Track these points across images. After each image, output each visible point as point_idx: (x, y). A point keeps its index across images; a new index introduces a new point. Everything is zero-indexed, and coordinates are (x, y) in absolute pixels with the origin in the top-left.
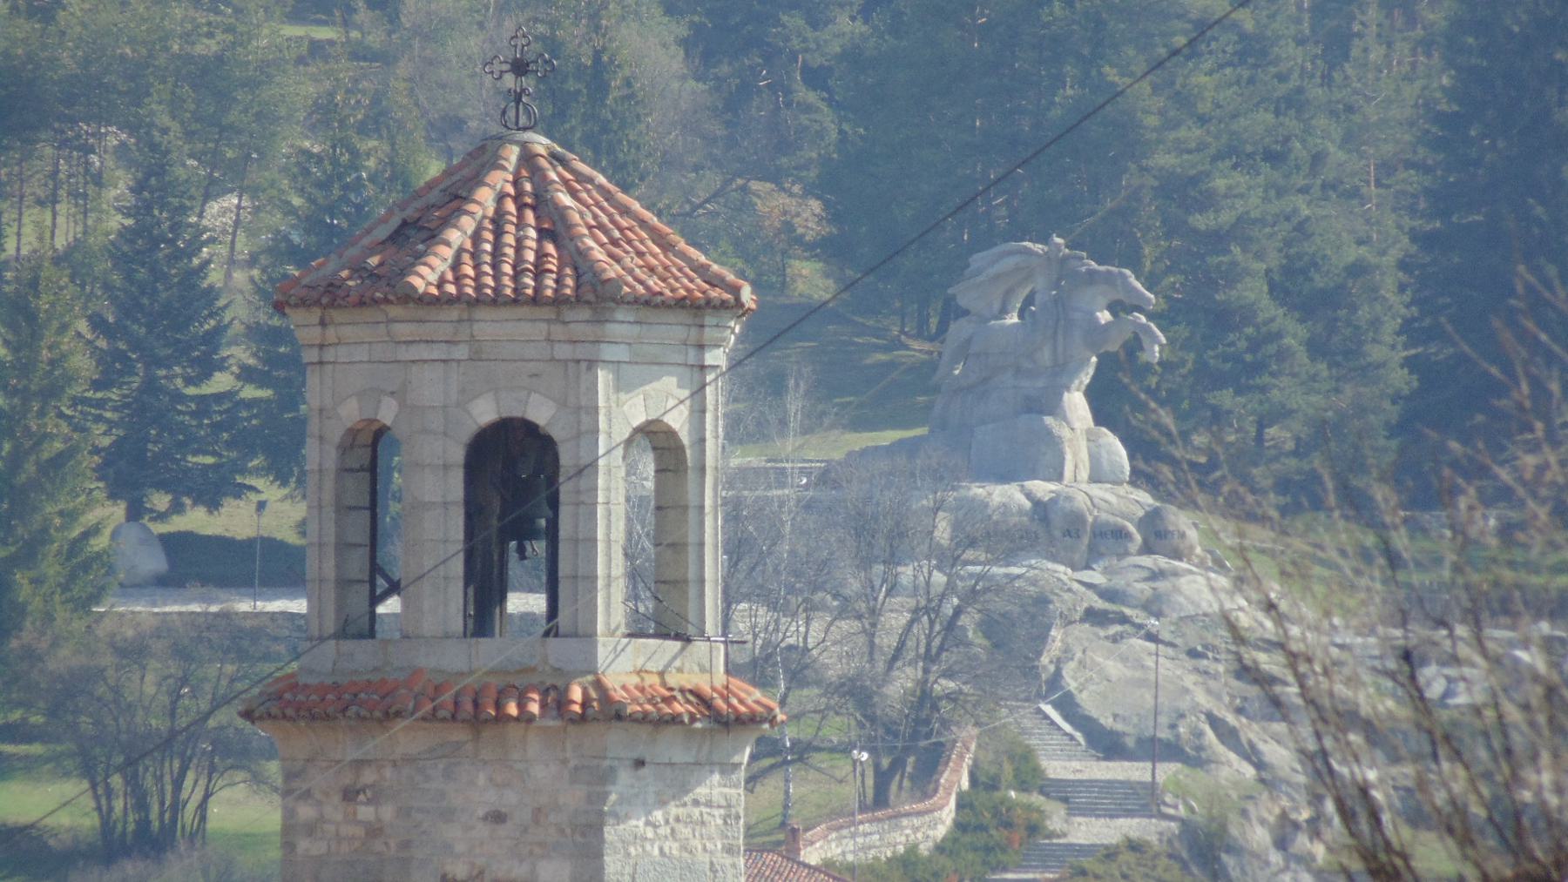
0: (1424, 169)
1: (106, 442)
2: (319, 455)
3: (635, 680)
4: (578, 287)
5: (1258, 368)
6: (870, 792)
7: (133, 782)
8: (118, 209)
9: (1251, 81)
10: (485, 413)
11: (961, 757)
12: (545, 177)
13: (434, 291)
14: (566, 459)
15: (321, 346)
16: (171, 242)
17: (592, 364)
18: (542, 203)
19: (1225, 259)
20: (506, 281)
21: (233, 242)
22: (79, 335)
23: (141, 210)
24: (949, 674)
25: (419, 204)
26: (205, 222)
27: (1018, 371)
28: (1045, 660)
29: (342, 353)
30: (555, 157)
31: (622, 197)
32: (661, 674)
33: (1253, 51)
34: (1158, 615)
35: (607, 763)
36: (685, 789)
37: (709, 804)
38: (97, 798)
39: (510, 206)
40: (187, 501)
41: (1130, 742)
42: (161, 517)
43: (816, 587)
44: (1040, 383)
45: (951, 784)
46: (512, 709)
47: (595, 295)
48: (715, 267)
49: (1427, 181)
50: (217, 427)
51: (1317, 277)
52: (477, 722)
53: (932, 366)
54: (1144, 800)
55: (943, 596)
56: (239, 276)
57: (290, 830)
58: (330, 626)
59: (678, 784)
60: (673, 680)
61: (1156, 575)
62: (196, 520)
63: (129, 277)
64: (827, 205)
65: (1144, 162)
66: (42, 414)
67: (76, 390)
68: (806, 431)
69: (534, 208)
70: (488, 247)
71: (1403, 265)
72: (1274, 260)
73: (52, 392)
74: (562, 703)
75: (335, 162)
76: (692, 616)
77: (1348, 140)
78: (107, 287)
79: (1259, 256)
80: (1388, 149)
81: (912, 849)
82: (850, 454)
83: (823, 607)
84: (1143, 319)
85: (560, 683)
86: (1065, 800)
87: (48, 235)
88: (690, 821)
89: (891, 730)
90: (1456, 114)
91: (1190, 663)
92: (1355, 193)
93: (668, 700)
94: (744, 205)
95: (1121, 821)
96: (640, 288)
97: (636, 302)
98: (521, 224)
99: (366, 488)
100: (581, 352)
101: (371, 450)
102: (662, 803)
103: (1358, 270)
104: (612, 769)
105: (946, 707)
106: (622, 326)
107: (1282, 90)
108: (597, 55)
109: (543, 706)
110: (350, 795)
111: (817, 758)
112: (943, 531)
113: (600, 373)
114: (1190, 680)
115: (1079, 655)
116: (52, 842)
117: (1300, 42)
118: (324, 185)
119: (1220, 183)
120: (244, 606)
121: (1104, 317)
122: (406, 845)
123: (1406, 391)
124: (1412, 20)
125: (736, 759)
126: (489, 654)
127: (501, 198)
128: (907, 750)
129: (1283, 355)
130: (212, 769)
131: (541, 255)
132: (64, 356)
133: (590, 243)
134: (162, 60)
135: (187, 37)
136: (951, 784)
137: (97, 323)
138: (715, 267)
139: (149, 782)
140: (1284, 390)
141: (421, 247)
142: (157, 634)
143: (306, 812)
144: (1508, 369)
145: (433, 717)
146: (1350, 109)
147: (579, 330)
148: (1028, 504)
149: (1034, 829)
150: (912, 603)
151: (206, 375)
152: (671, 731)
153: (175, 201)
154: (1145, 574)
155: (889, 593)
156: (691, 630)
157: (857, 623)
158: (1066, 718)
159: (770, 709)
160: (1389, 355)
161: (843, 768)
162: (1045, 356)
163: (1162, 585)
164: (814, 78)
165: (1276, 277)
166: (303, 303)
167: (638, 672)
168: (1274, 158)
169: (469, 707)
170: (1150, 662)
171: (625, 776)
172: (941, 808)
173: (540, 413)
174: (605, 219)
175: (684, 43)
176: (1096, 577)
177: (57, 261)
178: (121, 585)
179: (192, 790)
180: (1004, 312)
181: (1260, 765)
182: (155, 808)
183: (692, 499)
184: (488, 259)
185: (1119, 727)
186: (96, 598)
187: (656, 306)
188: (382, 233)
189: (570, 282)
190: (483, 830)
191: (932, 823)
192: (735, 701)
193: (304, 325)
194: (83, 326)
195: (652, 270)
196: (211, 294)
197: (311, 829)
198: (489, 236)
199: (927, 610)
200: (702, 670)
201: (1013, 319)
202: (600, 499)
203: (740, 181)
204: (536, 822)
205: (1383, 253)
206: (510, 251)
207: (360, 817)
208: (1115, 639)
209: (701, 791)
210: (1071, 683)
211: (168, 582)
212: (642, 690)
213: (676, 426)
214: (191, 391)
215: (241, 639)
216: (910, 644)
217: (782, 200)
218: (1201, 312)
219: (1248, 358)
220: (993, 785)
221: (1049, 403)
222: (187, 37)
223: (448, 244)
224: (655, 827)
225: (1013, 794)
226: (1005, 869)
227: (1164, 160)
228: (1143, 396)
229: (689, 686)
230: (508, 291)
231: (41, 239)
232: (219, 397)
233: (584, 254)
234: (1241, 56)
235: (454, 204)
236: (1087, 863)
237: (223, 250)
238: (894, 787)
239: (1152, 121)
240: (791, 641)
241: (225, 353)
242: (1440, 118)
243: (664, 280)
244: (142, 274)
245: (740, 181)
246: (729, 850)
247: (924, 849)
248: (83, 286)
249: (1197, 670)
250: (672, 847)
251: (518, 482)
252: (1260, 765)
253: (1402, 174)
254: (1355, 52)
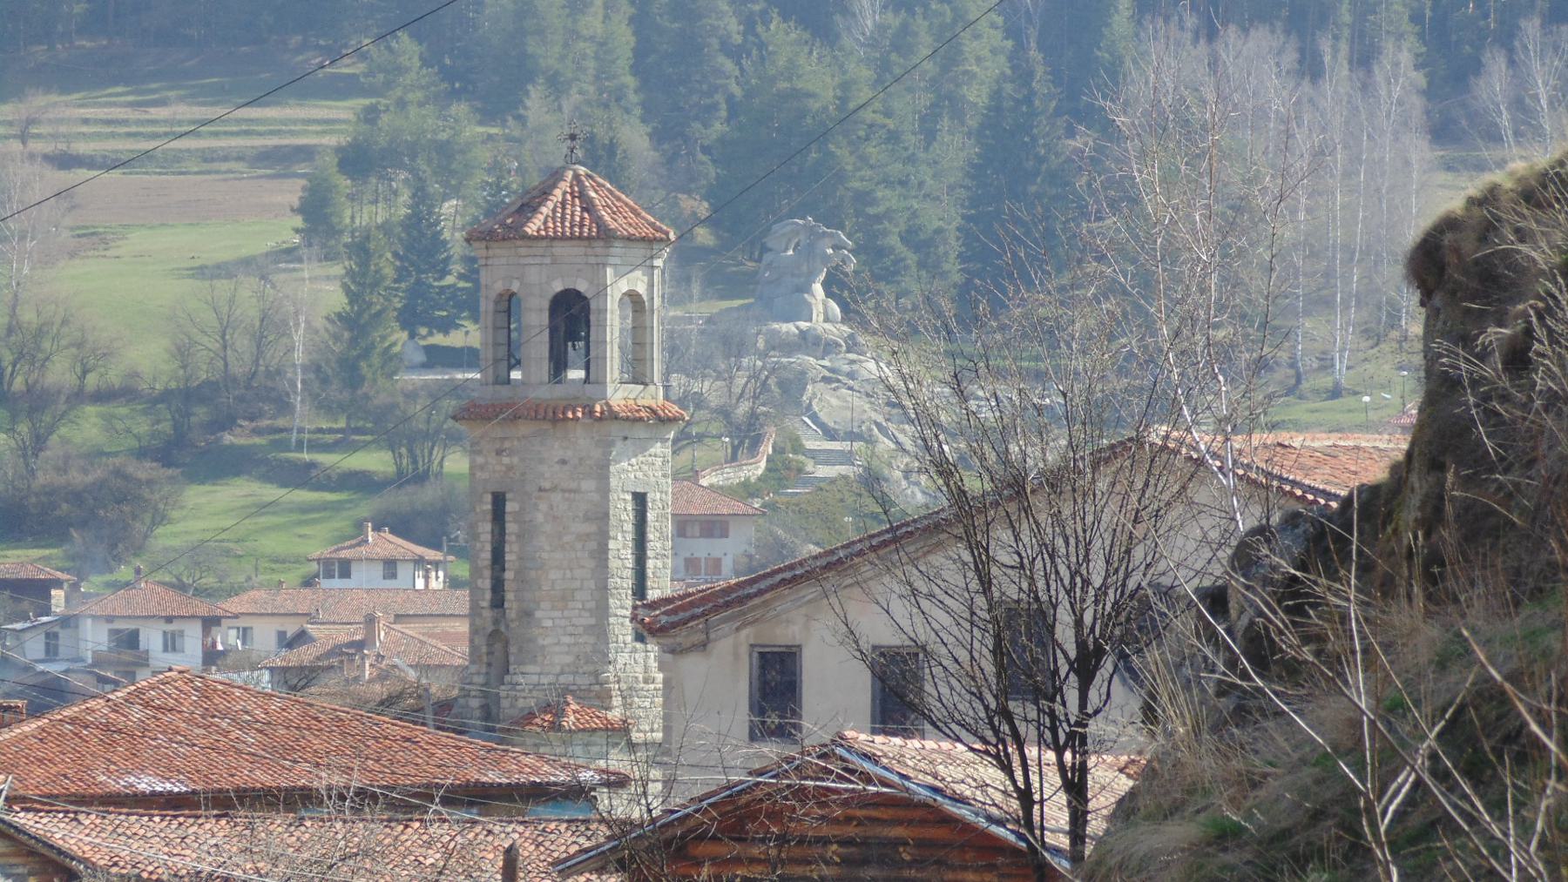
2: (486, 306)
5: (897, 273)
7: (410, 451)
10: (558, 287)
14: (593, 306)
17: (605, 265)
18: (582, 195)
27: (793, 275)
30: (588, 176)
33: (893, 137)
39: (569, 197)
42: (424, 338)
46: (570, 415)
47: (605, 235)
52: (555, 421)
53: (756, 273)
54: (847, 458)
56: (457, 235)
58: (491, 380)
61: (853, 362)
62: (438, 339)
67: (388, 283)
68: (701, 300)
71: (958, 229)
72: (903, 227)
73: (375, 285)
74: (592, 412)
78: (400, 239)
80: (952, 180)
89: (738, 428)
94: (676, 204)
97: (623, 238)
101: (508, 305)
103: (939, 231)
105: (762, 418)
106: (617, 249)
107: (905, 154)
110: (499, 453)
112: (761, 344)
117: (914, 133)
119: (879, 194)
120: (459, 376)
121: (830, 251)
122: (523, 474)
124: (963, 123)
126: (559, 391)
127: (565, 193)
129: (907, 268)
130: (445, 446)
131: (582, 219)
137: (396, 255)
139: (418, 452)
140: (908, 282)
143: (480, 460)
144: (1001, 246)
147: (599, 251)
149: (800, 470)
151: (441, 278)
152: (639, 425)
161: (718, 444)
162: (805, 268)
163: (855, 367)
164: (706, 150)
166: (479, 239)
168: (903, 183)
171: (619, 444)
173: (582, 287)
175: (650, 135)
176: (826, 363)
177: (378, 227)
180: (786, 249)
181: (897, 443)
182: (898, 832)
183: (648, 324)
186: (395, 373)
188: (513, 208)
190: (557, 467)
194: (389, 255)
196: (445, 242)
197: (482, 468)
201: (791, 252)
209: (652, 451)
210: (816, 408)
211: (427, 366)
215: (456, 389)
218: (870, 250)
220: (782, 451)
221: (806, 288)
222: (434, 132)
227: (856, 185)
232: (449, 287)
233: (600, 218)
234: (888, 141)
244: (415, 233)
246: (664, 476)
247: (753, 480)
250: (639, 475)
251: (572, 317)
252: (897, 443)
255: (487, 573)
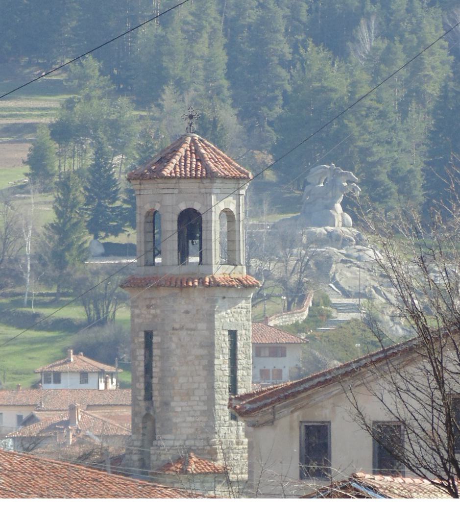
0: (427, 145)
1: (88, 219)
2: (140, 218)
3: (223, 276)
4: (207, 174)
5: (386, 197)
6: (286, 307)
7: (96, 307)
8: (91, 159)
9: (382, 123)
10: (183, 207)
11: (309, 298)
12: (198, 146)
13: (169, 175)
14: (204, 217)
15: (140, 190)
16: (105, 167)
17: (210, 194)
18: (197, 152)
19: (376, 169)
20: (188, 172)
21: (121, 168)
22: (81, 192)
23: (96, 160)
24: (306, 277)
25: (165, 153)
26: (113, 162)
28: (331, 272)
29: (146, 192)
30: (201, 140)
31: (218, 150)
32: (229, 274)
33: (382, 115)
34: (360, 260)
35: (215, 298)
36: (236, 304)
37: (242, 308)
38: (86, 311)
39: (189, 153)
40: (109, 234)
41: (353, 294)
42: (103, 238)
43: (272, 254)
44: (329, 201)
45: (307, 305)
46: (191, 284)
47: (211, 176)
48: (242, 168)
49: (428, 148)
50: (117, 215)
51: (400, 173)
52: (181, 287)
53: (301, 197)
54: (357, 308)
55: (304, 256)
56: (122, 176)
57: (133, 316)
59: (234, 303)
60: (232, 276)
61: (360, 250)
62: (112, 239)
63: (94, 176)
64: (273, 156)
65: (355, 144)
66: (71, 212)
67: (80, 206)
68: (268, 214)
69: (195, 153)
70: (183, 164)
71: (422, 170)
72: (389, 169)
73: (74, 206)
74: (204, 282)
75: (146, 146)
76: (237, 259)
77: (408, 138)
78: (88, 179)
79: (385, 168)
80: (418, 141)
81: (297, 322)
82: (280, 220)
83: (274, 259)
84: (355, 185)
85: (203, 277)
86: (336, 309)
87: (72, 166)
88: (237, 313)
89: (291, 291)
90: (436, 131)
91: (368, 273)
92: (409, 152)
93: (231, 281)
94: (252, 157)
95: (351, 314)
96: (223, 174)
98: (191, 158)
99: (152, 227)
100: (208, 191)
101: (153, 217)
102: (230, 308)
103: (410, 171)
104: (216, 299)
105: (305, 285)
106: (218, 184)
107: (390, 125)
108: (214, 119)
109: (198, 283)
110: (148, 307)
111: (273, 299)
112: (304, 240)
113: (213, 196)
114: (368, 277)
115: (340, 271)
116: (75, 323)
117: (395, 113)
118: (144, 152)
119: (374, 150)
120: (125, 261)
121: (345, 184)
122: (163, 320)
123: (423, 202)
124: (424, 107)
125: (249, 296)
126: (184, 269)
127: (186, 151)
128: (295, 296)
129: (391, 194)
131: (197, 166)
132: (77, 197)
133: (210, 162)
134: (102, 120)
135: (108, 115)
136: (307, 305)
137: (86, 189)
138: (242, 168)
139: (100, 307)
140: (392, 202)
141: (165, 164)
142: (102, 268)
143: (137, 311)
145: (170, 286)
146: (408, 130)
147: (207, 185)
148: (326, 233)
149: (328, 316)
150: (297, 258)
151: (114, 202)
153: (105, 157)
154: (433, 438)
155: (290, 256)
156: (237, 263)
157: (282, 264)
158: (337, 288)
159: (258, 283)
160: (419, 194)
161: (279, 301)
163: (361, 253)
164: (270, 124)
165: (390, 174)
166: (135, 179)
167: (224, 274)
168: (388, 143)
169: (179, 283)
170: (358, 273)
171: (220, 301)
172: (304, 311)
173: (197, 207)
174: (213, 156)
176: (344, 251)
177: (74, 172)
178: (93, 256)
179: (111, 308)
180: (319, 183)
182: (102, 314)
183: (237, 229)
184: (183, 167)
185: (350, 290)
186: (86, 259)
187: (227, 179)
188: (155, 160)
189: (204, 173)
191: (304, 315)
192: (248, 281)
193: (135, 185)
194: (82, 189)
195: (226, 169)
196: (115, 181)
197: (138, 316)
198: (183, 161)
199: (300, 260)
200: (240, 273)
201: (322, 185)
202: (213, 229)
203: (251, 151)
204: (197, 313)
205: (417, 167)
206: (189, 165)
207: (151, 312)
208: (349, 267)
209: (240, 305)
210: (338, 278)
211: (105, 255)
212: (224, 279)
213: (232, 210)
214: (110, 206)
215: (122, 269)
216: (296, 269)
217: (262, 155)
218: (370, 183)
219: (382, 194)
221: (332, 207)
222: (108, 115)
223: (173, 163)
224: (228, 314)
225: (323, 307)
226: (322, 327)
227: (360, 144)
228: (357, 213)
229: (237, 278)
230: (188, 175)
231: (70, 166)
232: (117, 207)
235: (174, 153)
236: (342, 324)
237: (118, 170)
238: (292, 306)
239: (357, 134)
240: (266, 268)
241: (119, 196)
242: (431, 132)
243: (229, 172)
245: (251, 151)
246: (247, 320)
247: (300, 322)
248: (82, 179)
249: (371, 275)
250: (233, 319)
251: (191, 225)
252: (387, 299)
253: (422, 146)
254: (409, 115)
255: (142, 380)
